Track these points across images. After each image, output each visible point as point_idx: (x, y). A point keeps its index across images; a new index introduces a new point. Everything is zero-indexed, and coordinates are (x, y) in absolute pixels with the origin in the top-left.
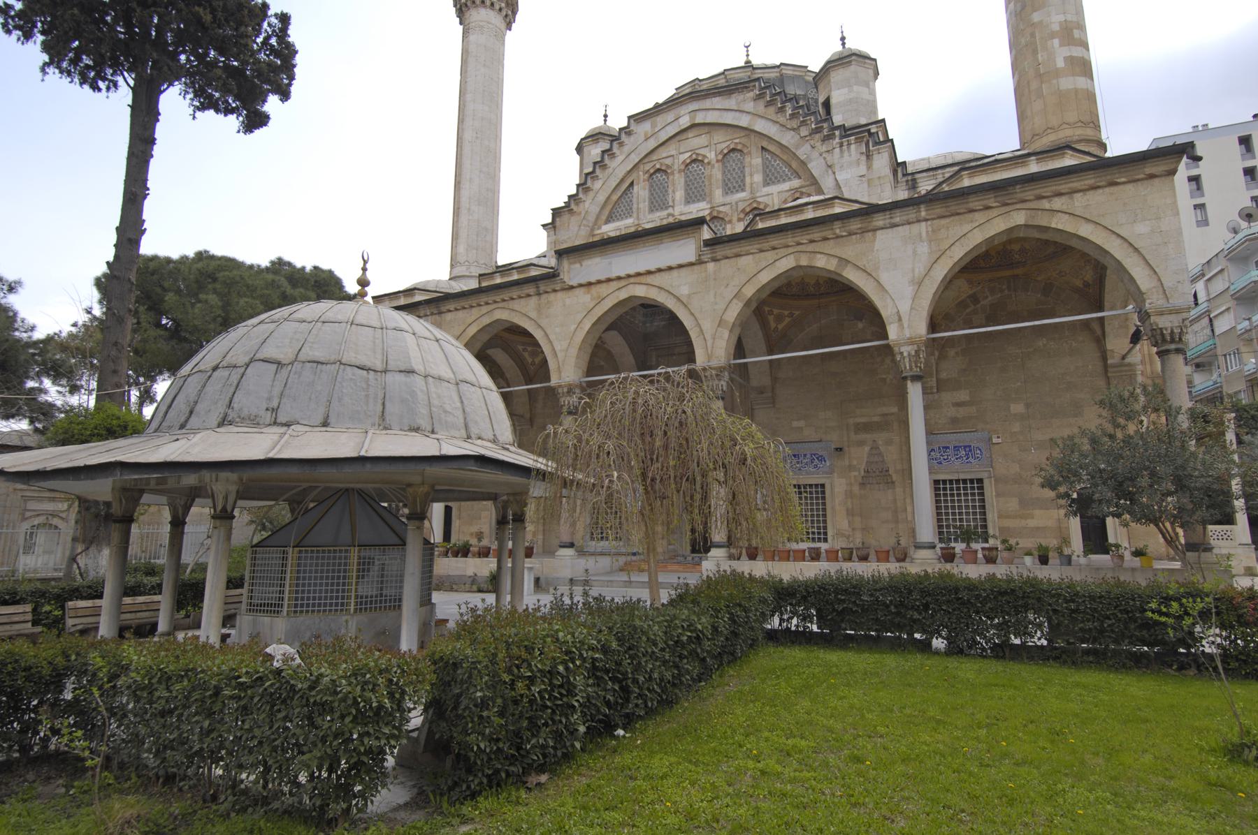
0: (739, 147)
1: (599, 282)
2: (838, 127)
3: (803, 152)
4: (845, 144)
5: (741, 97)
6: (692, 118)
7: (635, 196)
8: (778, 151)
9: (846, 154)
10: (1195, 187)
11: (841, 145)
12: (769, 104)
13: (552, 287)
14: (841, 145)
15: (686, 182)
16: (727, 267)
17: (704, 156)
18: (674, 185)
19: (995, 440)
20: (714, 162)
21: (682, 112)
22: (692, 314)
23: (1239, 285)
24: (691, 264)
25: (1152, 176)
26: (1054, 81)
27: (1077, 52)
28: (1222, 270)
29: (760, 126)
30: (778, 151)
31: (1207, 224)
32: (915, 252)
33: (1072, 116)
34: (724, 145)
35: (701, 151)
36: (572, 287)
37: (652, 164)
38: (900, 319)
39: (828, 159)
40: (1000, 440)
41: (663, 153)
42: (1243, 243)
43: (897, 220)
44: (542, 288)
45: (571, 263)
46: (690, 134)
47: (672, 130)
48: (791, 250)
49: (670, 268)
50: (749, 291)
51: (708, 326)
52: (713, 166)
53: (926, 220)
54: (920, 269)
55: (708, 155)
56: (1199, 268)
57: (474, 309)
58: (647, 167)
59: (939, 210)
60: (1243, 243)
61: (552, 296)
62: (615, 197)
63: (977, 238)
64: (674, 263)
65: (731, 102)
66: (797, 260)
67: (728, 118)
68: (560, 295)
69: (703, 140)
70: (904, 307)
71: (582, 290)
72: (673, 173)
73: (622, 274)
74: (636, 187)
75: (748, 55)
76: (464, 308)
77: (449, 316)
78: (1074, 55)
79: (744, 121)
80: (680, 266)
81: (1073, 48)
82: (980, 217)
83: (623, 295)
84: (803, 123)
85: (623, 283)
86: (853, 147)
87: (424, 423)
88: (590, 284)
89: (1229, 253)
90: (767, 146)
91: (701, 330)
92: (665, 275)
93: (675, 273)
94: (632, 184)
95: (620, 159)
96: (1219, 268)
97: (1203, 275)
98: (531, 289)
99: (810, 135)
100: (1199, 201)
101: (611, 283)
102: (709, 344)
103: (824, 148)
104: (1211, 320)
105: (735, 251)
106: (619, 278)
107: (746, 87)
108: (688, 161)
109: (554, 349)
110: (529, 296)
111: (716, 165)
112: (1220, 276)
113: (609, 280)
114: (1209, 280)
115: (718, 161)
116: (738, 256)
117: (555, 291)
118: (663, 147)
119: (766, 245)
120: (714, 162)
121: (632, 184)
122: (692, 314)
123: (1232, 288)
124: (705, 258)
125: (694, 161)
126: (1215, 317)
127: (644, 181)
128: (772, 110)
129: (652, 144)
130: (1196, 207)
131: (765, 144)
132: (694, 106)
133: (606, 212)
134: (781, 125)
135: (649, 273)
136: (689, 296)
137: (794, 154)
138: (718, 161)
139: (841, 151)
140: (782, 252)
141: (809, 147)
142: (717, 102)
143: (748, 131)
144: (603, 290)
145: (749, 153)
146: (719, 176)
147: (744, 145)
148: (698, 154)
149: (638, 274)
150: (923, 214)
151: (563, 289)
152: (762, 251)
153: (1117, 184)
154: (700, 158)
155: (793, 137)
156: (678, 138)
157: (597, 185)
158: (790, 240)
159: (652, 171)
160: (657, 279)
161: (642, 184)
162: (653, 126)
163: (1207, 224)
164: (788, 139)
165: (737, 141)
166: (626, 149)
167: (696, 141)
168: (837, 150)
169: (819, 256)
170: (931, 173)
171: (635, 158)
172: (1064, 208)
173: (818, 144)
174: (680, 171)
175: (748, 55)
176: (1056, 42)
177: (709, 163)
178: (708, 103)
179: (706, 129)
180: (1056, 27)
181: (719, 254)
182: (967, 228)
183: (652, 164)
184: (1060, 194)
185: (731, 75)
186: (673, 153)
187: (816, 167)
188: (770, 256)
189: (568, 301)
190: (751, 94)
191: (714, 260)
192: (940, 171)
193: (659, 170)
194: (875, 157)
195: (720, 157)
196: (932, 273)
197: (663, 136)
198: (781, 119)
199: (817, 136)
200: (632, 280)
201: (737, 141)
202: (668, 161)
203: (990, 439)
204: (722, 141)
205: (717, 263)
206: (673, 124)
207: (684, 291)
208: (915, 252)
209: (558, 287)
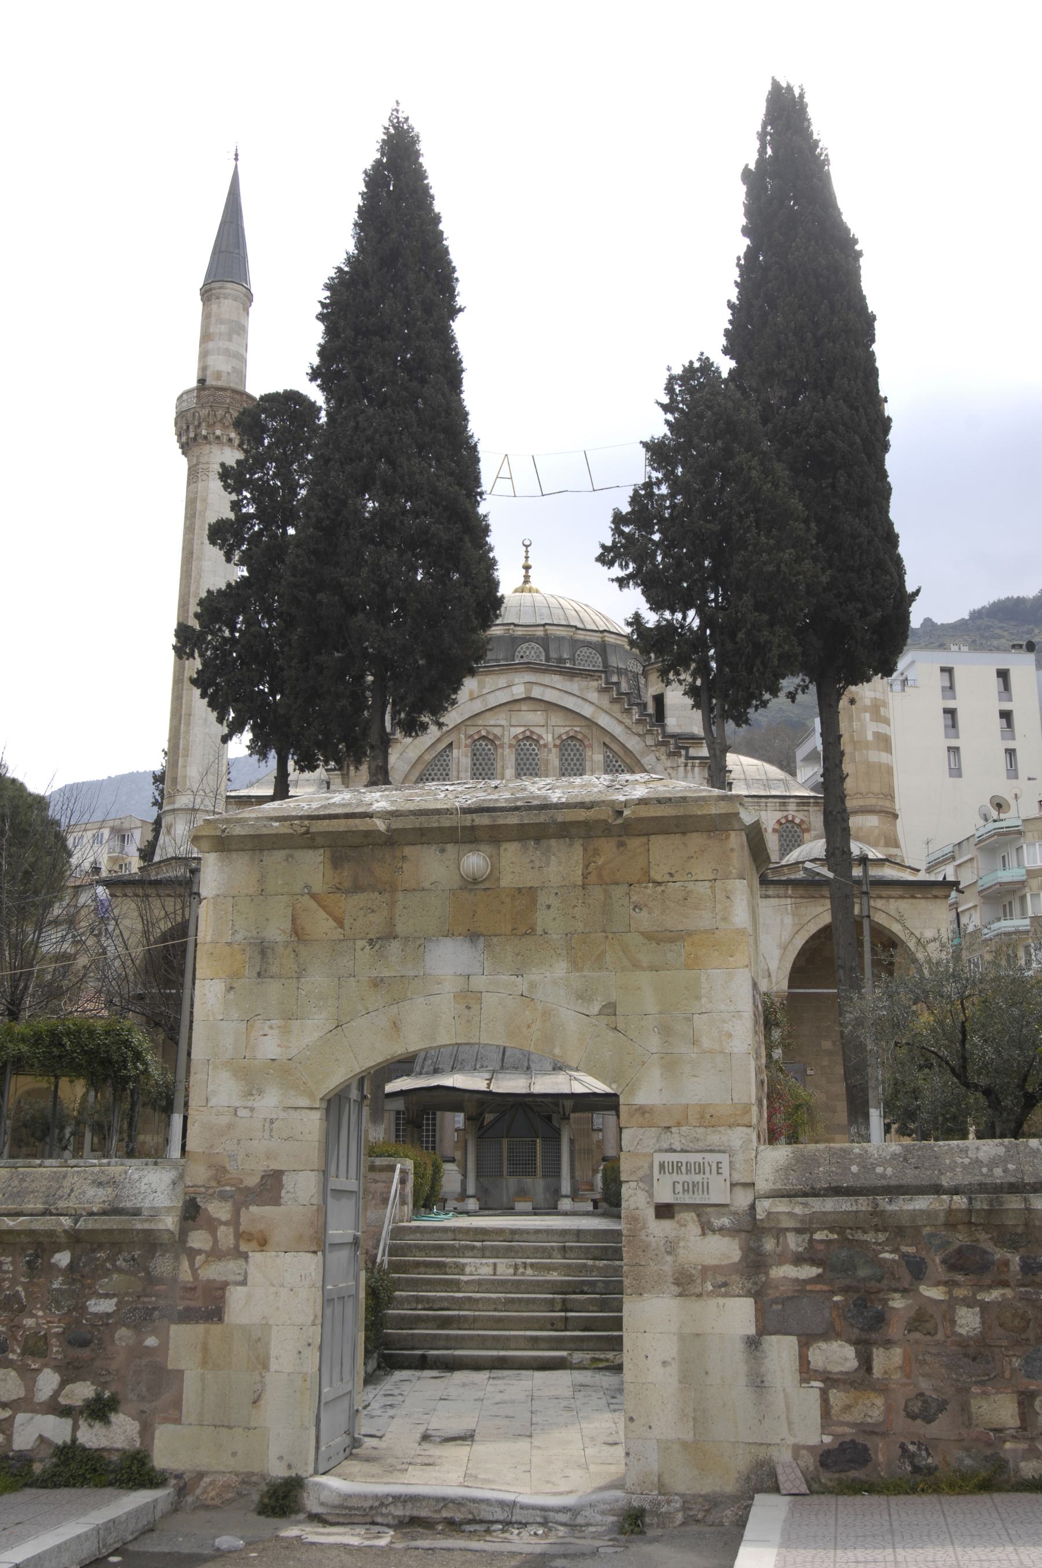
0: (579, 737)
5: (584, 683)
6: (528, 690)
7: (455, 761)
8: (621, 753)
9: (690, 775)
10: (950, 723)
11: (686, 765)
12: (614, 701)
14: (686, 765)
15: (517, 760)
17: (540, 737)
18: (503, 759)
19: (809, 1072)
20: (551, 746)
21: (517, 681)
23: (988, 881)
25: (936, 897)
26: (865, 752)
27: (882, 728)
28: (971, 859)
29: (604, 721)
30: (621, 753)
31: (960, 776)
32: (782, 921)
33: (876, 788)
34: (563, 730)
37: (477, 729)
38: (770, 976)
40: (812, 1072)
41: (491, 720)
42: (992, 836)
43: (770, 893)
46: (524, 707)
47: (503, 697)
52: (550, 751)
53: (791, 897)
54: (786, 936)
55: (544, 736)
56: (950, 849)
58: (472, 731)
59: (801, 891)
60: (992, 836)
62: (428, 757)
65: (574, 686)
67: (570, 703)
70: (773, 965)
72: (502, 746)
75: (527, 558)
78: (880, 731)
79: (587, 711)
81: (880, 724)
84: (650, 732)
86: (697, 769)
89: (980, 842)
90: (609, 744)
96: (969, 856)
97: (953, 858)
99: (656, 746)
100: (953, 743)
103: (669, 764)
104: (958, 914)
108: (521, 737)
111: (554, 750)
112: (969, 865)
114: (959, 866)
115: (555, 746)
118: (491, 713)
123: (980, 883)
125: (528, 738)
126: (963, 912)
127: (466, 746)
128: (616, 707)
130: (949, 749)
131: (607, 741)
133: (416, 773)
134: (626, 727)
137: (639, 761)
138: (555, 746)
139: (685, 770)
141: (655, 760)
142: (556, 680)
143: (590, 723)
145: (591, 746)
148: (531, 732)
150: (790, 892)
153: (916, 898)
154: (535, 737)
155: (638, 743)
156: (508, 707)
159: (476, 737)
161: (463, 749)
163: (960, 776)
165: (578, 729)
167: (534, 718)
168: (682, 769)
170: (756, 800)
172: (883, 908)
173: (663, 757)
174: (511, 746)
175: (527, 558)
176: (868, 715)
177: (545, 746)
179: (543, 706)
180: (868, 702)
183: (477, 729)
184: (881, 897)
185: (552, 630)
186: (503, 723)
190: (595, 684)
192: (763, 800)
193: (484, 738)
195: (558, 742)
196: (794, 941)
197: (493, 701)
198: (627, 721)
199: (663, 749)
202: (497, 731)
203: (805, 1070)
206: (505, 690)
208: (782, 921)
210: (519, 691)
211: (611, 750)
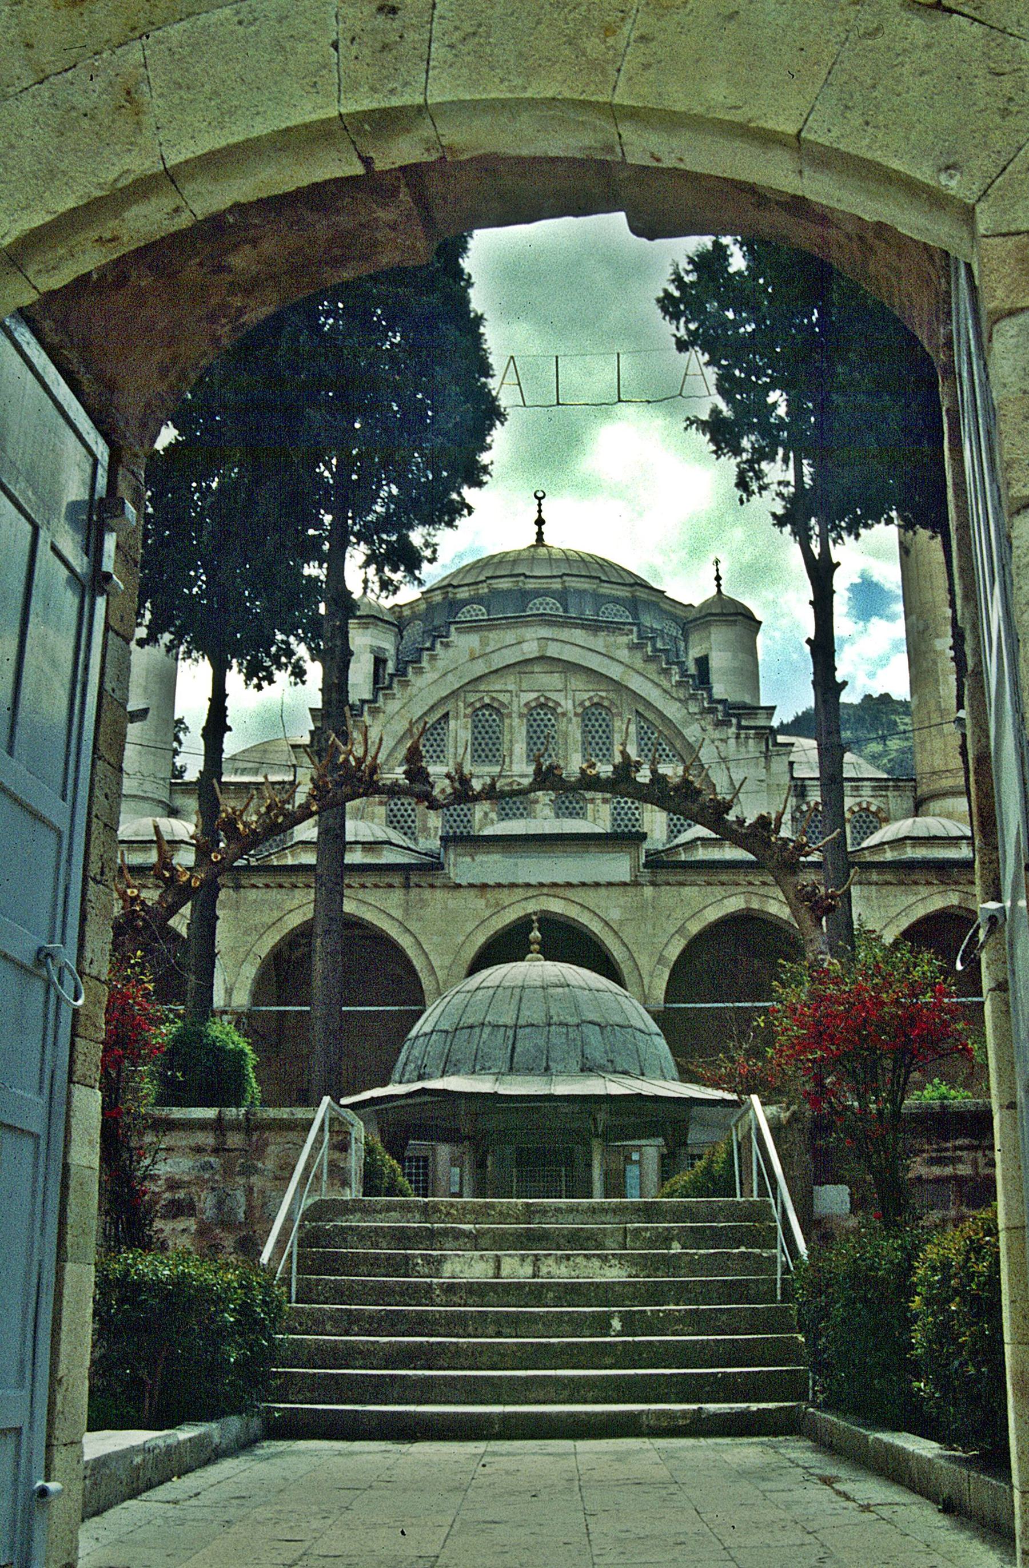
0: (606, 703)
1: (499, 885)
2: (720, 701)
3: (692, 732)
4: (743, 736)
7: (452, 734)
8: (658, 722)
13: (430, 880)
14: (738, 737)
15: (528, 732)
16: (668, 896)
17: (558, 704)
18: (511, 733)
22: (625, 944)
24: (625, 884)
29: (636, 683)
30: (658, 722)
34: (586, 696)
35: (554, 696)
36: (459, 886)
37: (479, 695)
39: (721, 748)
44: (414, 879)
45: (457, 855)
47: (511, 657)
48: (740, 889)
49: (597, 885)
50: (694, 928)
51: (644, 961)
55: (563, 703)
57: (297, 891)
58: (472, 698)
61: (427, 894)
63: (920, 912)
64: (603, 880)
65: (599, 642)
66: (746, 902)
67: (593, 662)
68: (439, 894)
69: (555, 680)
71: (473, 892)
73: (533, 881)
74: (452, 723)
76: (281, 886)
77: (252, 894)
79: (615, 672)
80: (610, 884)
82: (924, 891)
83: (532, 907)
84: (693, 697)
85: (531, 892)
86: (751, 741)
87: (602, 1060)
88: (485, 886)
91: (637, 965)
92: (591, 893)
93: (603, 891)
94: (446, 716)
95: (430, 676)
98: (397, 880)
101: (516, 890)
102: (646, 981)
103: (717, 735)
105: (681, 878)
106: (528, 885)
107: (620, 629)
109: (430, 963)
110: (390, 886)
111: (574, 719)
113: (513, 885)
116: (682, 884)
117: (432, 886)
119: (714, 879)
120: (571, 715)
121: (446, 716)
122: (625, 944)
124: (641, 880)
125: (542, 706)
128: (652, 667)
129: (480, 668)
132: (545, 632)
135: (569, 885)
136: (621, 923)
137: (681, 733)
138: (576, 715)
140: (733, 889)
143: (619, 686)
144: (505, 897)
146: (579, 736)
147: (612, 703)
148: (547, 699)
149: (555, 885)
151: (445, 886)
152: (709, 884)
154: (551, 704)
155: (679, 709)
156: (517, 669)
157: (392, 707)
158: (741, 878)
159: (478, 705)
160: (590, 897)
162: (484, 643)
164: (673, 710)
165: (604, 694)
166: (440, 664)
169: (772, 901)
171: (454, 682)
173: (709, 728)
174: (521, 716)
178: (565, 634)
181: (661, 878)
182: (912, 899)
187: (707, 755)
188: (719, 891)
189: (452, 904)
191: (653, 884)
194: (774, 759)
195: (579, 710)
200: (545, 890)
201: (604, 694)
202: (504, 698)
204: (583, 692)
205: (657, 888)
207: (614, 915)
209: (438, 883)
210: (531, 649)
211: (646, 719)
